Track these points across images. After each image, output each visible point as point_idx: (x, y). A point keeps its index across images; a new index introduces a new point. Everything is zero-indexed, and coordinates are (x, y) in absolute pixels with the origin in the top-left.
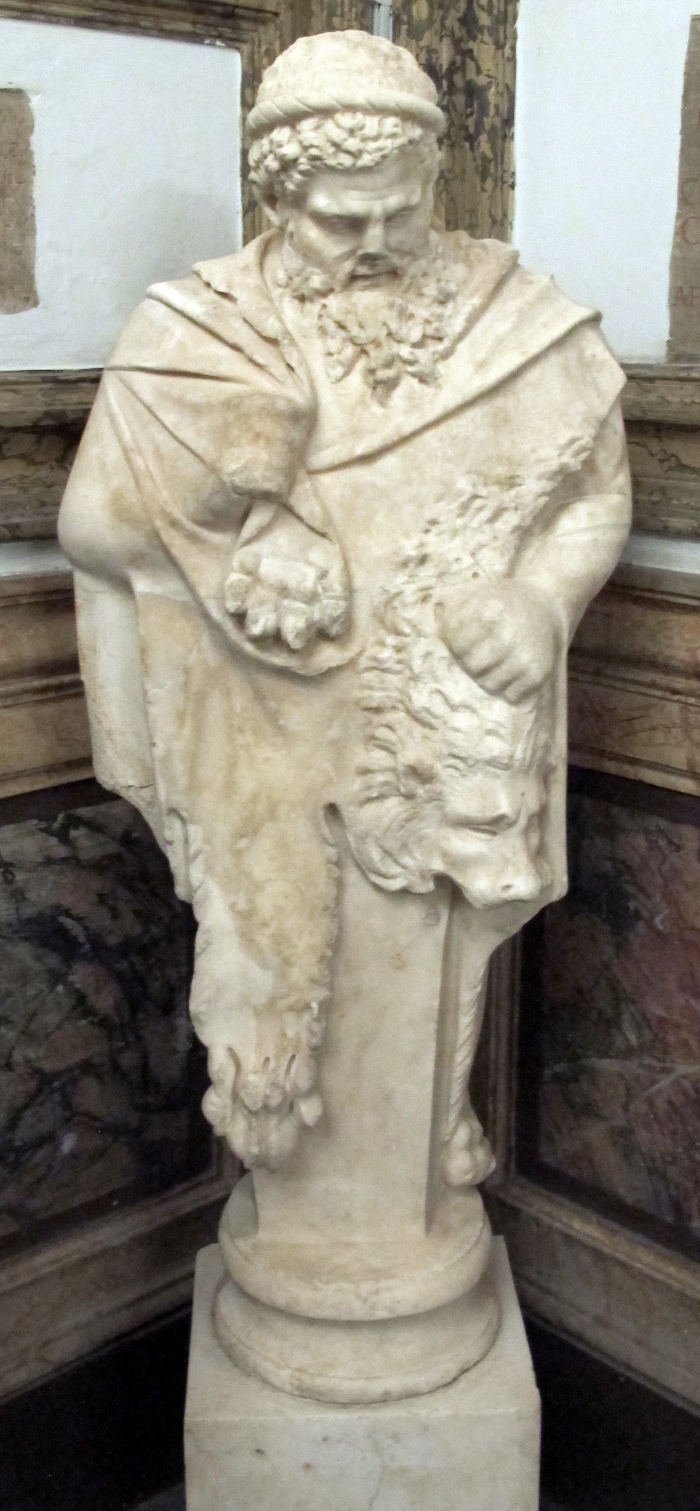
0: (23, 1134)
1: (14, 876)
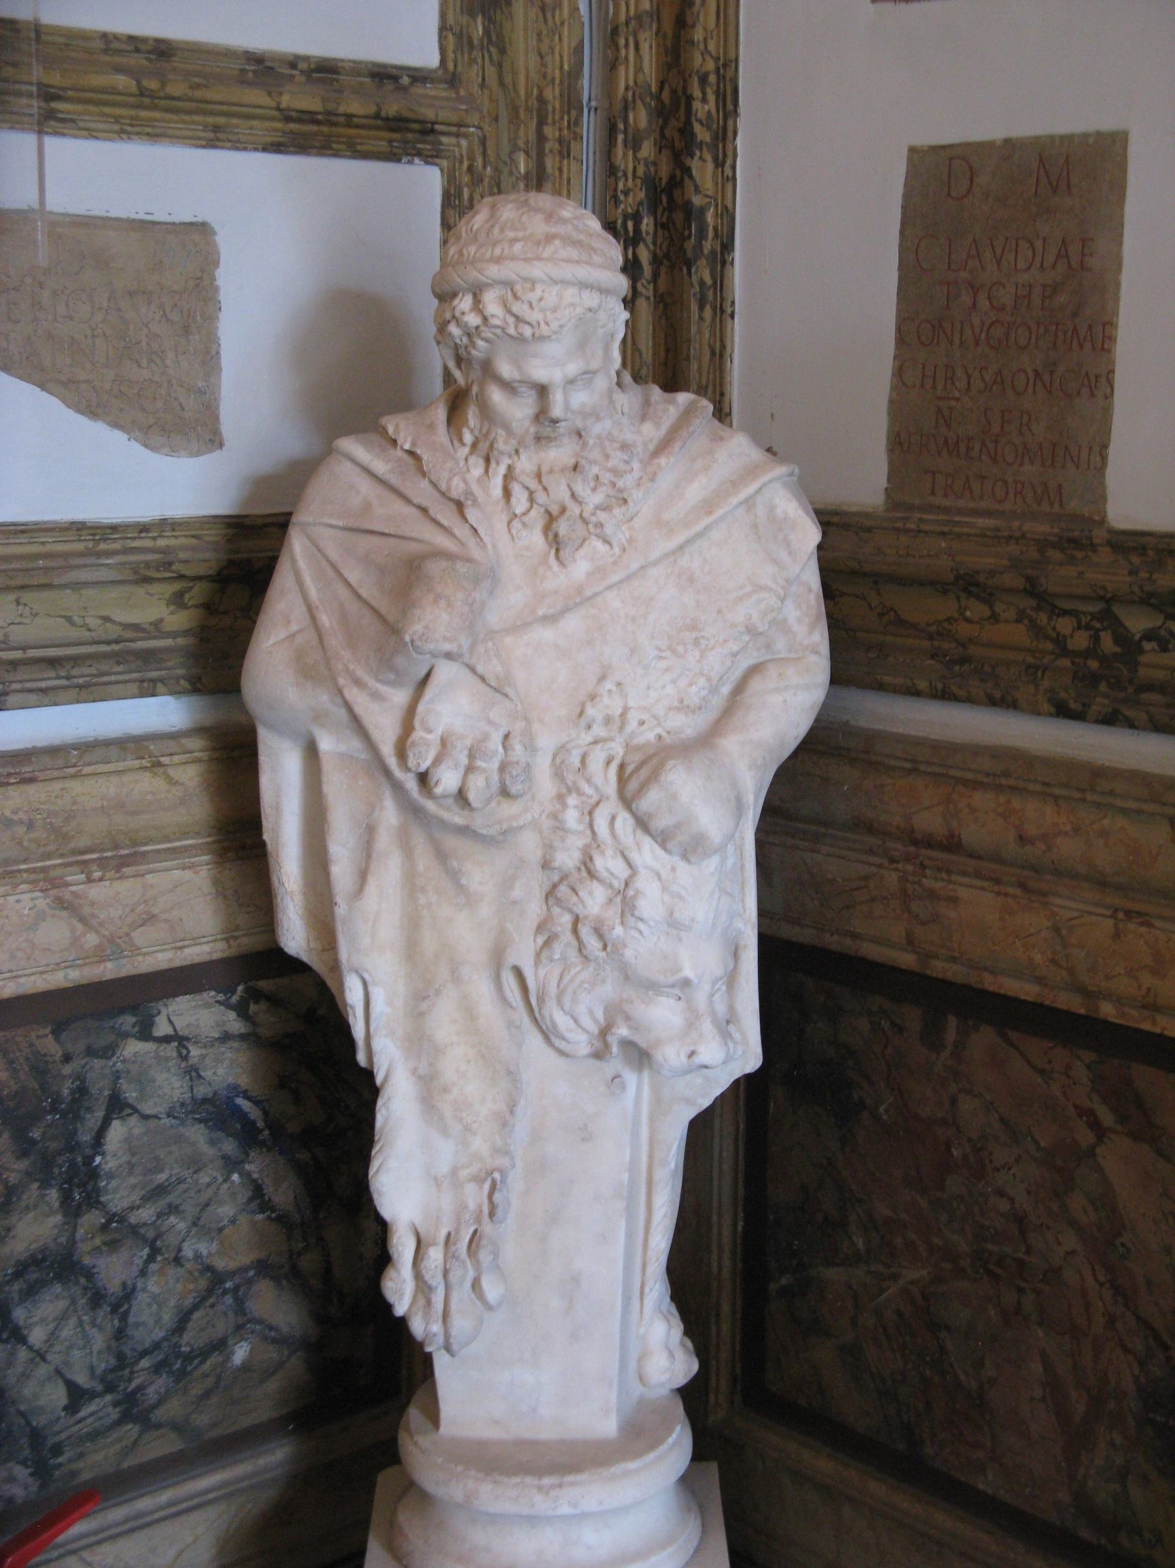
0: (190, 1339)
1: (189, 1052)
